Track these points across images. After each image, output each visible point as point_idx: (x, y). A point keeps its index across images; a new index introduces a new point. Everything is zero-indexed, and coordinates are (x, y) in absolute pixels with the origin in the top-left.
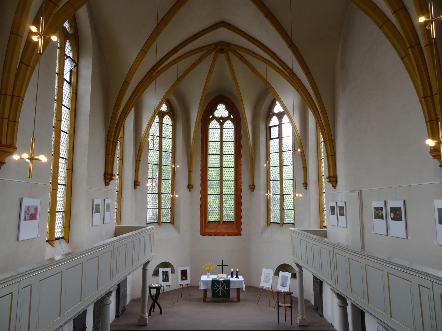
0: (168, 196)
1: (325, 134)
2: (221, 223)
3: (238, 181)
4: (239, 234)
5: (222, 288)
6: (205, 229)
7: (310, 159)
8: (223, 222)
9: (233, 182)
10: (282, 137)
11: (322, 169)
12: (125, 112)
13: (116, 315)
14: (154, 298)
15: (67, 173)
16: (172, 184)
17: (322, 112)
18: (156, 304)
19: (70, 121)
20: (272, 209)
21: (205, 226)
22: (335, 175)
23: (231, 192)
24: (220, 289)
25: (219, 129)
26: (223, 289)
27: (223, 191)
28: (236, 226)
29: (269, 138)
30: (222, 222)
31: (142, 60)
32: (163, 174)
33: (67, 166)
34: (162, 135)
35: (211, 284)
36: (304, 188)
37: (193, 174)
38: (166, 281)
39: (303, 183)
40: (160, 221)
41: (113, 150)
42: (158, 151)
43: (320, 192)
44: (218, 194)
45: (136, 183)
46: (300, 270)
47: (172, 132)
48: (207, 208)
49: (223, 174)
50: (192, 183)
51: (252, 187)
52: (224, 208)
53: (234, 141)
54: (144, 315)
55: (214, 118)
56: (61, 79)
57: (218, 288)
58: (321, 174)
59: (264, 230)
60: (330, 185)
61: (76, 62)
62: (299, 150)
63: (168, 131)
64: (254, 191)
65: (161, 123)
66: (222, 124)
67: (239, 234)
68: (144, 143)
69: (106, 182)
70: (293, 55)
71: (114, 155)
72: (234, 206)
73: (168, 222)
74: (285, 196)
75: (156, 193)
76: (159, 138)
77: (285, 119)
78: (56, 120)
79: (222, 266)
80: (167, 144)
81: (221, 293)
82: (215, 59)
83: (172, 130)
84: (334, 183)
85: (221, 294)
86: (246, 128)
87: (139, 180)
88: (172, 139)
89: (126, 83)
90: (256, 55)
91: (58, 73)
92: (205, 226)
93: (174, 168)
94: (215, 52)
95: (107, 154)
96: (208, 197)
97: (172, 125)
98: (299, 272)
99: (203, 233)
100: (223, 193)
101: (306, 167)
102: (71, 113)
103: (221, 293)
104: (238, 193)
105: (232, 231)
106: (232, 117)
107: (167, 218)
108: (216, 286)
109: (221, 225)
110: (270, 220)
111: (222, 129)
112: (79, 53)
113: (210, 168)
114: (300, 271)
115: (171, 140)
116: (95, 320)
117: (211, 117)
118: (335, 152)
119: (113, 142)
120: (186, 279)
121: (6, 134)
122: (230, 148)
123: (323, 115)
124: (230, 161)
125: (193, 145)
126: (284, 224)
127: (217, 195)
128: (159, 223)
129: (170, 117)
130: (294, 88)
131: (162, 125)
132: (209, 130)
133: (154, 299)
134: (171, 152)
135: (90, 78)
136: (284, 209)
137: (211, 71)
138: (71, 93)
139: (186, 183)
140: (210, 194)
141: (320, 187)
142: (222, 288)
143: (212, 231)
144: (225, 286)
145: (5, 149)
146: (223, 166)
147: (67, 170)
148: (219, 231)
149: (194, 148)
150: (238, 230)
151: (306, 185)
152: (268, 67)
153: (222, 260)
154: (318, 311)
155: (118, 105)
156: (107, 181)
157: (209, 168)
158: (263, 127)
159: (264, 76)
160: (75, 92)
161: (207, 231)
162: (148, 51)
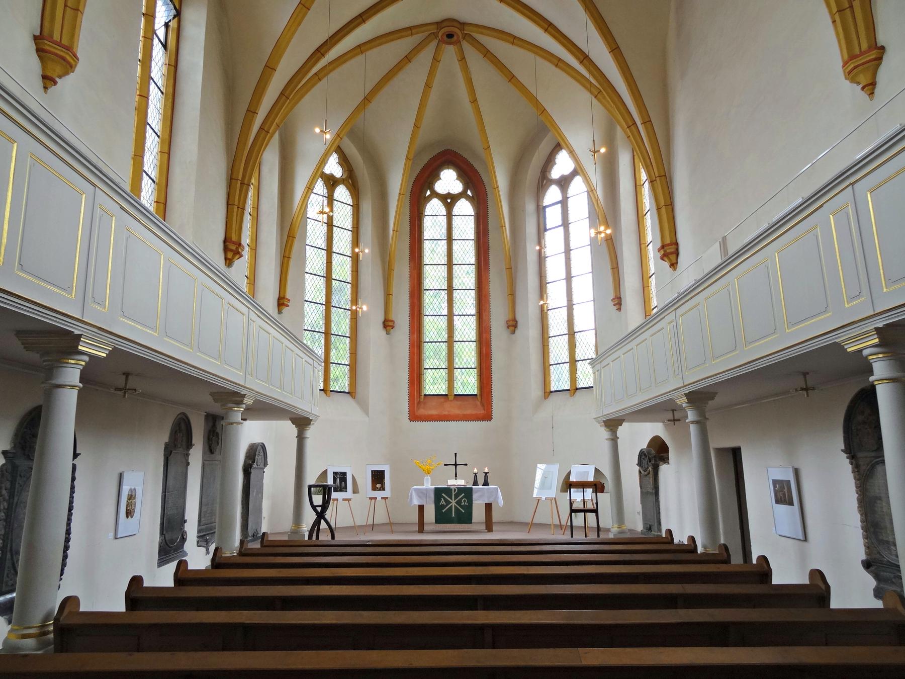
2: (451, 398)
4: (488, 417)
5: (456, 503)
6: (418, 408)
8: (455, 395)
9: (474, 317)
10: (572, 275)
13: (241, 540)
14: (319, 509)
15: (155, 208)
16: (351, 319)
17: (644, 123)
18: (322, 521)
19: (164, 115)
20: (553, 365)
21: (419, 403)
22: (675, 241)
23: (471, 336)
24: (451, 505)
25: (445, 217)
26: (457, 506)
27: (453, 335)
28: (481, 402)
29: (541, 229)
30: (453, 397)
31: (299, 24)
32: (333, 297)
33: (155, 194)
35: (432, 496)
36: (615, 308)
37: (393, 299)
38: (341, 491)
39: (612, 300)
40: (329, 387)
41: (243, 195)
42: (325, 279)
43: (644, 275)
44: (445, 342)
45: (281, 301)
46: (613, 436)
47: (351, 218)
48: (423, 369)
51: (513, 325)
52: (456, 368)
53: (476, 264)
54: (299, 528)
55: (435, 194)
56: (150, 33)
57: (448, 503)
58: (648, 270)
60: (666, 264)
62: (603, 150)
63: (343, 215)
64: (516, 332)
65: (331, 199)
66: (449, 207)
67: (488, 417)
68: (299, 224)
70: (589, 16)
74: (577, 335)
75: (321, 331)
76: (328, 226)
77: (577, 186)
79: (456, 465)
80: (342, 268)
81: (453, 514)
82: (436, 60)
83: (351, 220)
84: (673, 257)
85: (453, 516)
86: (500, 217)
87: (288, 296)
88: (351, 231)
89: (269, 68)
91: (146, 14)
92: (419, 403)
93: (356, 310)
94: (433, 44)
98: (612, 439)
99: (414, 417)
100: (454, 339)
101: (618, 267)
102: (166, 100)
103: (453, 514)
104: (484, 337)
105: (474, 412)
106: (469, 193)
107: (340, 379)
108: (443, 500)
109: (451, 401)
110: (550, 387)
111: (449, 216)
113: (428, 290)
114: (611, 437)
115: (349, 259)
116: (204, 509)
117: (428, 193)
119: (242, 183)
120: (383, 488)
121: (60, 26)
122: (466, 252)
123: (646, 129)
124: (466, 277)
127: (442, 344)
129: (348, 188)
131: (332, 230)
132: (425, 219)
133: (320, 511)
134: (350, 255)
136: (576, 361)
137: (428, 86)
138: (166, 64)
139: (381, 318)
140: (427, 340)
142: (456, 503)
143: (434, 412)
144: (462, 498)
145: (57, 49)
146: (454, 286)
147: (155, 203)
148: (446, 413)
150: (484, 410)
151: (618, 302)
152: (538, 58)
153: (456, 454)
154: (651, 531)
155: (252, 111)
156: (230, 255)
157: (425, 290)
158: (530, 207)
159: (532, 90)
160: (173, 63)
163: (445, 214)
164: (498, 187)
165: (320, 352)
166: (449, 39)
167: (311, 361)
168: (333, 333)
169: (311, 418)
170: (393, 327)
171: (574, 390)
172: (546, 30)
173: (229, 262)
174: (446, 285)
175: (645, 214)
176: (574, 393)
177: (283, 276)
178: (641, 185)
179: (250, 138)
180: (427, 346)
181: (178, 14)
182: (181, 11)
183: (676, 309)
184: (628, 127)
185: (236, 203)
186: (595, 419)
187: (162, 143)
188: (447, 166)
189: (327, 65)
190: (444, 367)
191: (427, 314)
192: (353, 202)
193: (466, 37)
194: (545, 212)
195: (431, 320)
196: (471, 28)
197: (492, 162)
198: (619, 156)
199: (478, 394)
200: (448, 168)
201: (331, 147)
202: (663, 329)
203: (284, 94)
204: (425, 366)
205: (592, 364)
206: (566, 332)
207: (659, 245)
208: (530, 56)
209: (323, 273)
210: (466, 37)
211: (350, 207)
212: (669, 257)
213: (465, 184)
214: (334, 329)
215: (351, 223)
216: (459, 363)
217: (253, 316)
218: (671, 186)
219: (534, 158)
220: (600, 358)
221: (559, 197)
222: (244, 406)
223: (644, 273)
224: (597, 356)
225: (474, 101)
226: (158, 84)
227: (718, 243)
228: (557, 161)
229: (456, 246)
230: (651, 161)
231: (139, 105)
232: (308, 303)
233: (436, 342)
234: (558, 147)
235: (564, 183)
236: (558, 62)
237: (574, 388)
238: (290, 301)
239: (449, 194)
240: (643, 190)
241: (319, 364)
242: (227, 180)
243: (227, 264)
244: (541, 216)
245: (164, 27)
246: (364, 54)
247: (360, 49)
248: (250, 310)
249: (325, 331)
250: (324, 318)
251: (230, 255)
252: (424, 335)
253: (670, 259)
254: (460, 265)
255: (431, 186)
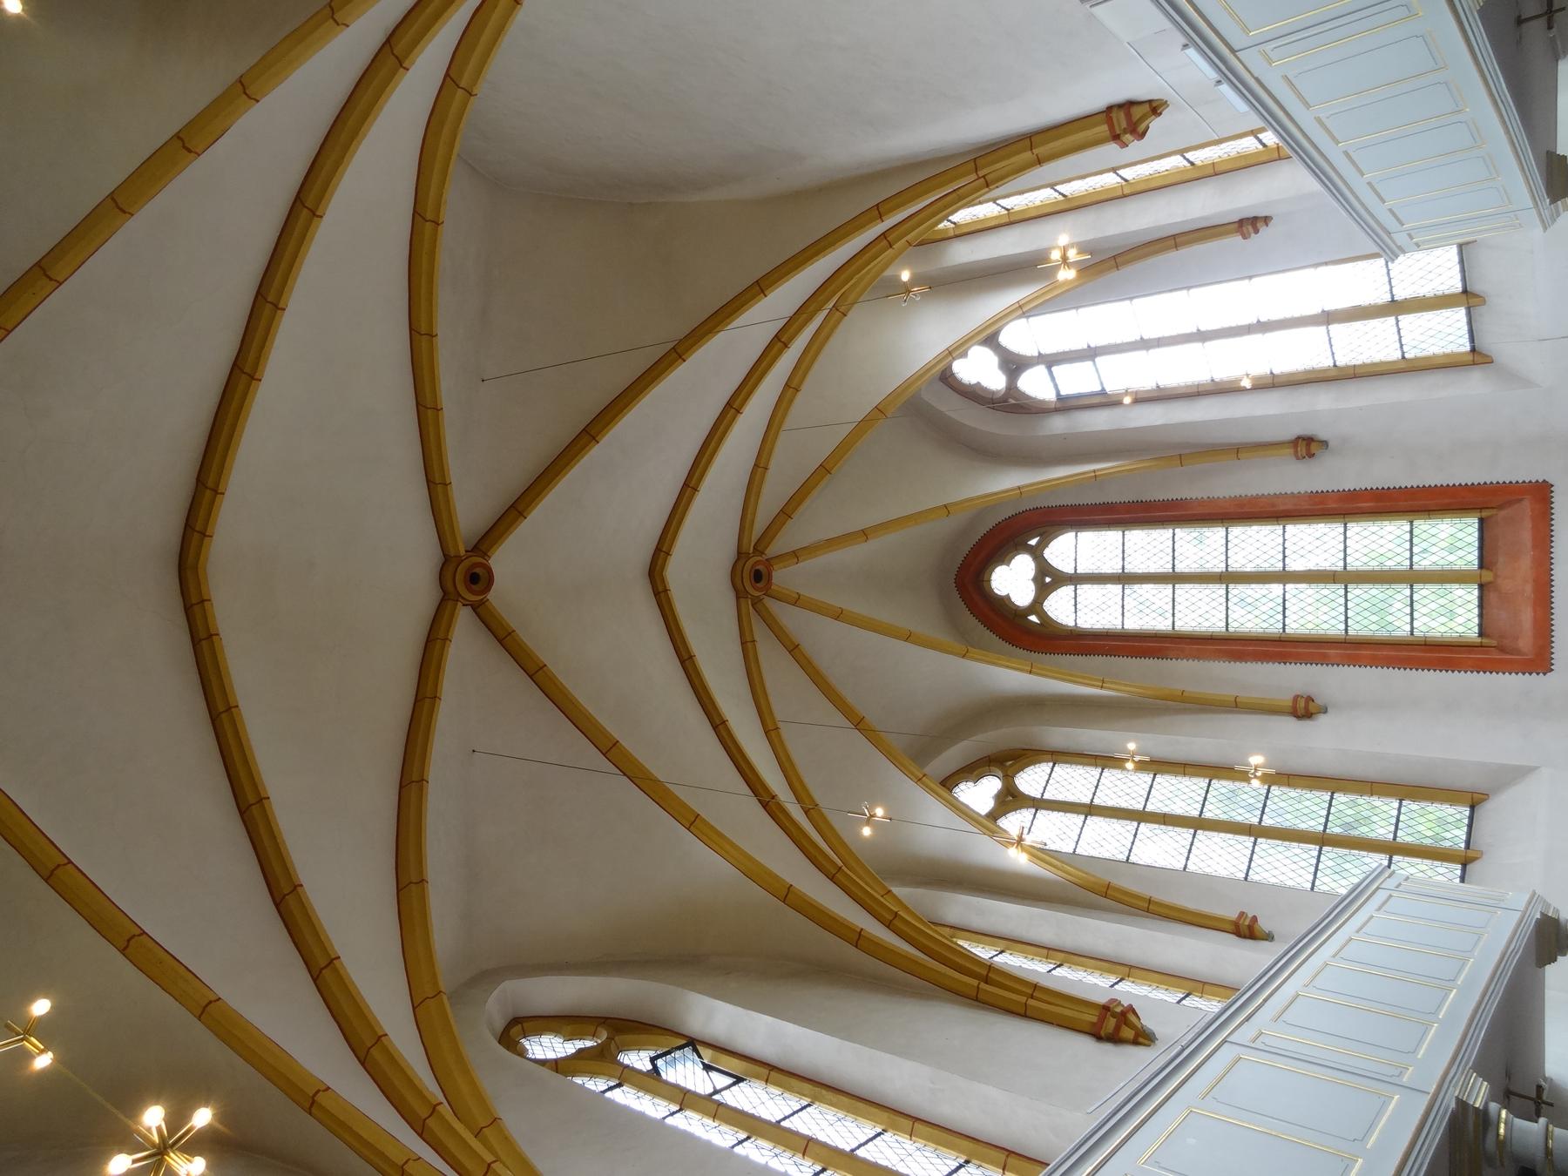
0: (1342, 807)
1: (961, 191)
2: (1487, 576)
3: (1281, 508)
4: (1541, 493)
6: (1518, 652)
7: (1134, 228)
8: (1481, 566)
11: (1166, 173)
12: (891, 918)
16: (1289, 785)
17: (881, 217)
21: (1501, 649)
25: (1078, 586)
28: (1500, 507)
29: (1104, 401)
30: (1485, 572)
34: (1084, 805)
39: (1245, 237)
42: (1199, 832)
43: (1264, 158)
44: (1346, 588)
48: (1411, 638)
49: (1446, 568)
50: (1286, 699)
51: (1307, 446)
52: (1411, 565)
55: (1037, 605)
58: (1183, 171)
59: (1513, 378)
60: (1156, 125)
61: (684, 1042)
63: (1072, 782)
64: (1322, 435)
65: (1039, 804)
66: (1061, 579)
67: (1541, 493)
69: (1132, 1038)
71: (1034, 989)
72: (1404, 522)
73: (1471, 818)
76: (1092, 815)
78: (804, 1155)
80: (1177, 793)
82: (797, 601)
84: (1137, 112)
87: (1232, 915)
88: (1155, 775)
89: (788, 896)
90: (760, 467)
92: (1501, 649)
94: (769, 602)
95: (1025, 1014)
96: (1360, 633)
97: (1051, 764)
99: (1540, 661)
100: (1339, 569)
101: (1174, 236)
104: (1334, 506)
106: (1033, 542)
109: (1496, 576)
111: (1076, 579)
112: (669, 1028)
113: (1227, 624)
117: (1033, 618)
118: (1001, 142)
119: (987, 980)
125: (1123, 688)
126: (1468, 289)
128: (1466, 859)
130: (715, 328)
132: (1082, 626)
135: (740, 1010)
137: (839, 615)
139: (1290, 723)
140: (1342, 627)
141: (1243, 163)
143: (1527, 616)
148: (1529, 588)
149: (1135, 687)
150: (1522, 499)
151: (1250, 224)
155: (858, 939)
156: (1127, 1033)
158: (1058, 425)
160: (764, 1071)
161: (1526, 643)
162: (694, 811)
163: (1072, 587)
164: (1019, 488)
165: (1377, 860)
166: (764, 578)
167: (1381, 896)
168: (1321, 828)
169: (1538, 916)
170: (1310, 699)
171: (1468, 297)
172: (738, 412)
173: (1143, 1038)
174: (1218, 586)
175: (1064, 196)
176: (1476, 296)
177: (1189, 918)
178: (1008, 214)
179: (904, 951)
180: (1354, 627)
181: (693, 1043)
182: (691, 1038)
183: (1233, 51)
184: (891, 247)
185: (1023, 999)
186: (1545, 228)
187: (897, 1129)
188: (985, 584)
189: (759, 800)
190: (1408, 592)
191: (1281, 626)
192: (1047, 761)
193: (759, 549)
194: (1068, 398)
195: (1295, 617)
196: (745, 541)
197: (972, 499)
198: (956, 263)
199: (1479, 515)
200: (989, 581)
201: (937, 794)
202: (1286, 78)
203: (833, 875)
204: (1404, 634)
205: (1393, 252)
206: (1323, 328)
207: (1112, 147)
208: (783, 441)
209: (1187, 834)
210: (759, 549)
211: (1055, 769)
212: (1138, 120)
213: (1016, 550)
214: (1315, 825)
215: (1088, 769)
216: (1399, 559)
217: (1246, 1034)
218: (994, 144)
219: (967, 423)
220: (1377, 235)
221: (1040, 370)
222: (1493, 1106)
223: (1185, 178)
224: (1381, 252)
225: (865, 534)
226: (795, 1109)
227: (1095, 9)
228: (973, 382)
229: (1134, 566)
230: (949, 193)
231: (820, 1161)
232: (1251, 872)
233: (1347, 609)
234: (947, 378)
235: (1014, 365)
236: (791, 387)
237: (1464, 297)
238: (1244, 913)
239: (1035, 580)
240: (1016, 208)
241: (1389, 877)
242: (978, 1007)
243: (1146, 1042)
244: (1075, 403)
245: (710, 1073)
246: (780, 725)
247: (771, 731)
248: (1230, 1039)
249: (1316, 844)
250: (1287, 843)
251: (1127, 1033)
252: (1329, 632)
253: (1143, 118)
254: (1174, 558)
255: (1020, 614)
